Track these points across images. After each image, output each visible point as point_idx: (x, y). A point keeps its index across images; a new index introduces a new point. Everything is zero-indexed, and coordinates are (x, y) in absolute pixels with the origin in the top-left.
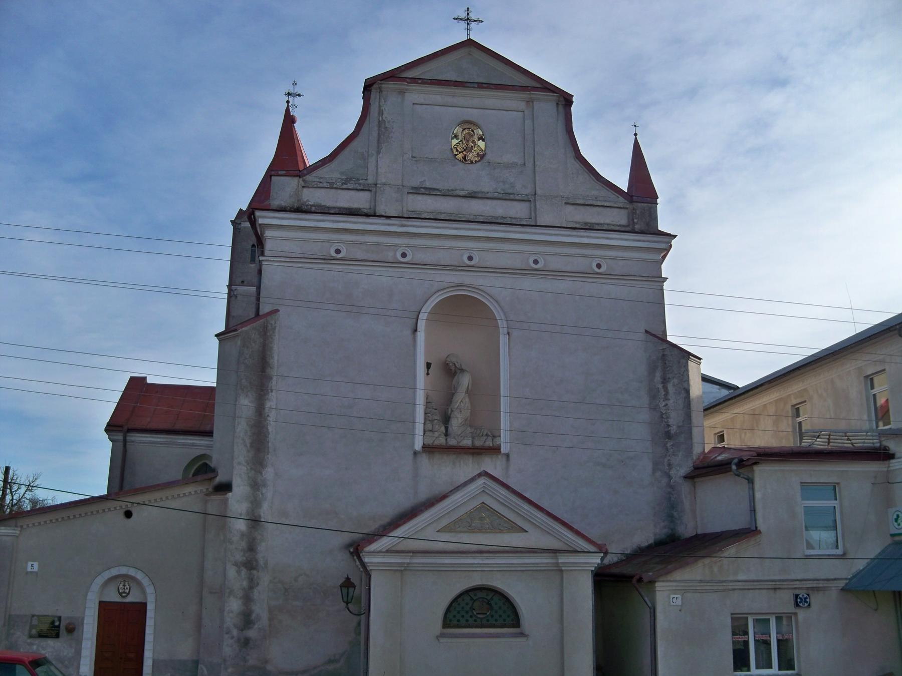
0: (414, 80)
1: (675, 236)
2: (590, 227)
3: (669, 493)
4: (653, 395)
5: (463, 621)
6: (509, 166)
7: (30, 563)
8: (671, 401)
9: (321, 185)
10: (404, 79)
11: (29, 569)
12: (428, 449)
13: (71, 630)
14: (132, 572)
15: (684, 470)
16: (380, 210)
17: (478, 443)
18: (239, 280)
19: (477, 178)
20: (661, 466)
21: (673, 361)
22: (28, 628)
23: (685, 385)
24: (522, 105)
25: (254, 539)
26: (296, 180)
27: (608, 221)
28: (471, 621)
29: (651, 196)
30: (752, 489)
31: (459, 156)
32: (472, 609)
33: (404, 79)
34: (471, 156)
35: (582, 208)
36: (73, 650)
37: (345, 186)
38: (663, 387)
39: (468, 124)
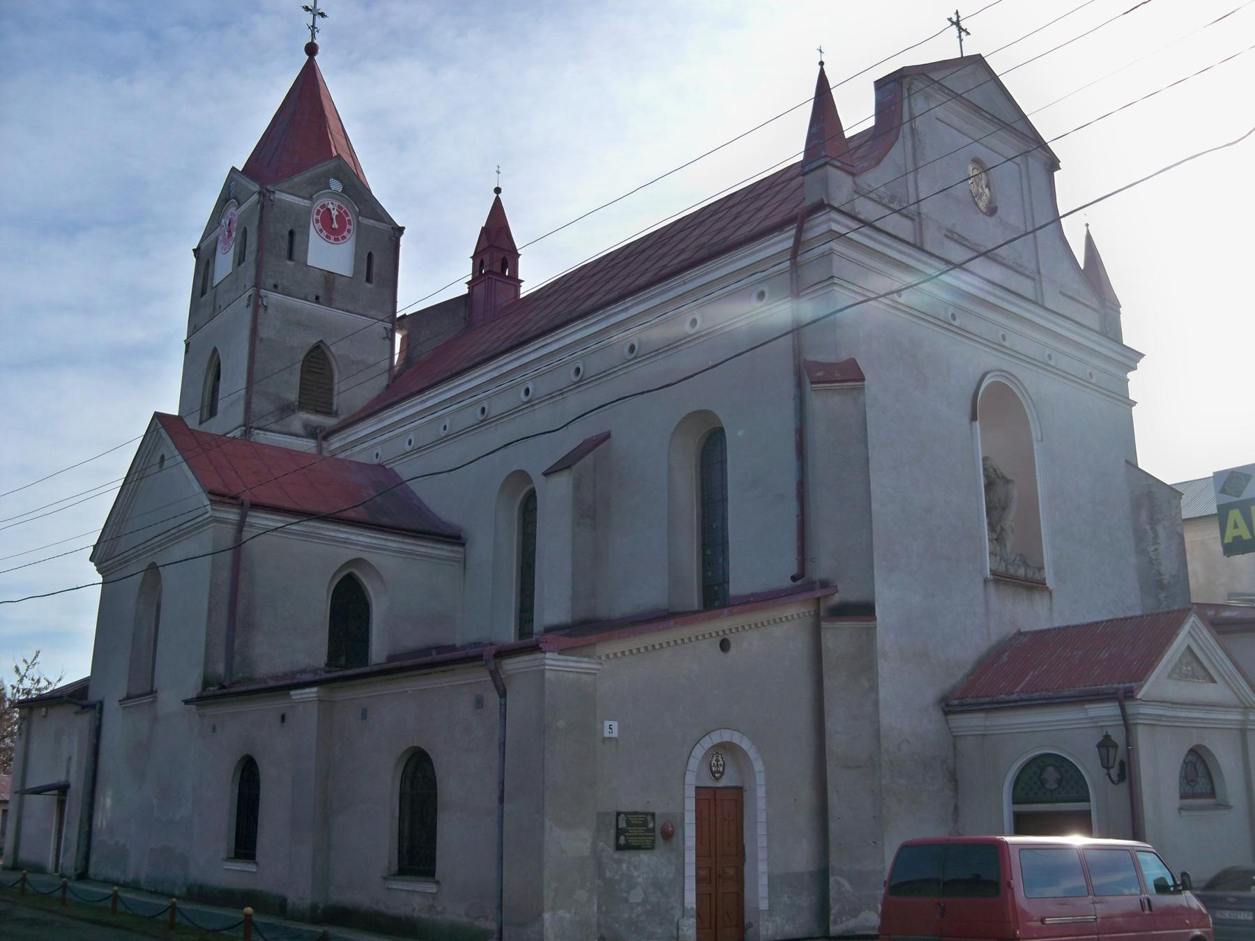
7: (607, 723)
8: (1162, 547)
11: (607, 735)
13: (668, 836)
22: (613, 832)
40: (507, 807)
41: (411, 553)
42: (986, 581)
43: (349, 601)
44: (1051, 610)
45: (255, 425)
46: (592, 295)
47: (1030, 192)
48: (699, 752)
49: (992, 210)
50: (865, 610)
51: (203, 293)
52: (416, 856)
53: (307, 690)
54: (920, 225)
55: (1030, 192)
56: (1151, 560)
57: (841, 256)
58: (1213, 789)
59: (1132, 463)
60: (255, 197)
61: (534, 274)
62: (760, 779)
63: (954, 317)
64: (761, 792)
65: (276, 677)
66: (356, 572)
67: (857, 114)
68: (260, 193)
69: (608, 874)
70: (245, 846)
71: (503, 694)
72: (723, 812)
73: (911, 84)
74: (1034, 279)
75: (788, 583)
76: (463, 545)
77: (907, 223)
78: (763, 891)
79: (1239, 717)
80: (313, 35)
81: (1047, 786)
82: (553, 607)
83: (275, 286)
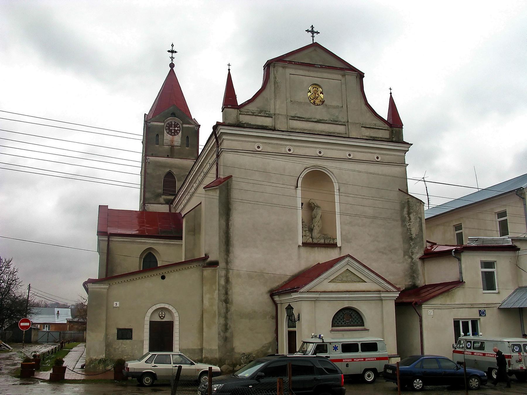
0: (290, 62)
1: (412, 144)
2: (374, 139)
3: (412, 266)
4: (403, 220)
5: (340, 324)
6: (337, 107)
7: (115, 303)
9: (248, 113)
10: (286, 61)
11: (115, 306)
12: (305, 244)
14: (167, 306)
15: (420, 254)
16: (278, 127)
17: (327, 242)
19: (319, 113)
20: (408, 253)
21: (410, 205)
23: (419, 216)
24: (340, 77)
25: (227, 288)
26: (236, 110)
27: (380, 136)
28: (343, 323)
29: (400, 125)
30: (460, 263)
31: (312, 101)
32: (343, 318)
33: (286, 61)
34: (317, 102)
35: (369, 130)
37: (260, 115)
38: (408, 216)
39: (316, 85)
41: (168, 244)
52: (292, 348)
66: (152, 252)
80: (172, 60)
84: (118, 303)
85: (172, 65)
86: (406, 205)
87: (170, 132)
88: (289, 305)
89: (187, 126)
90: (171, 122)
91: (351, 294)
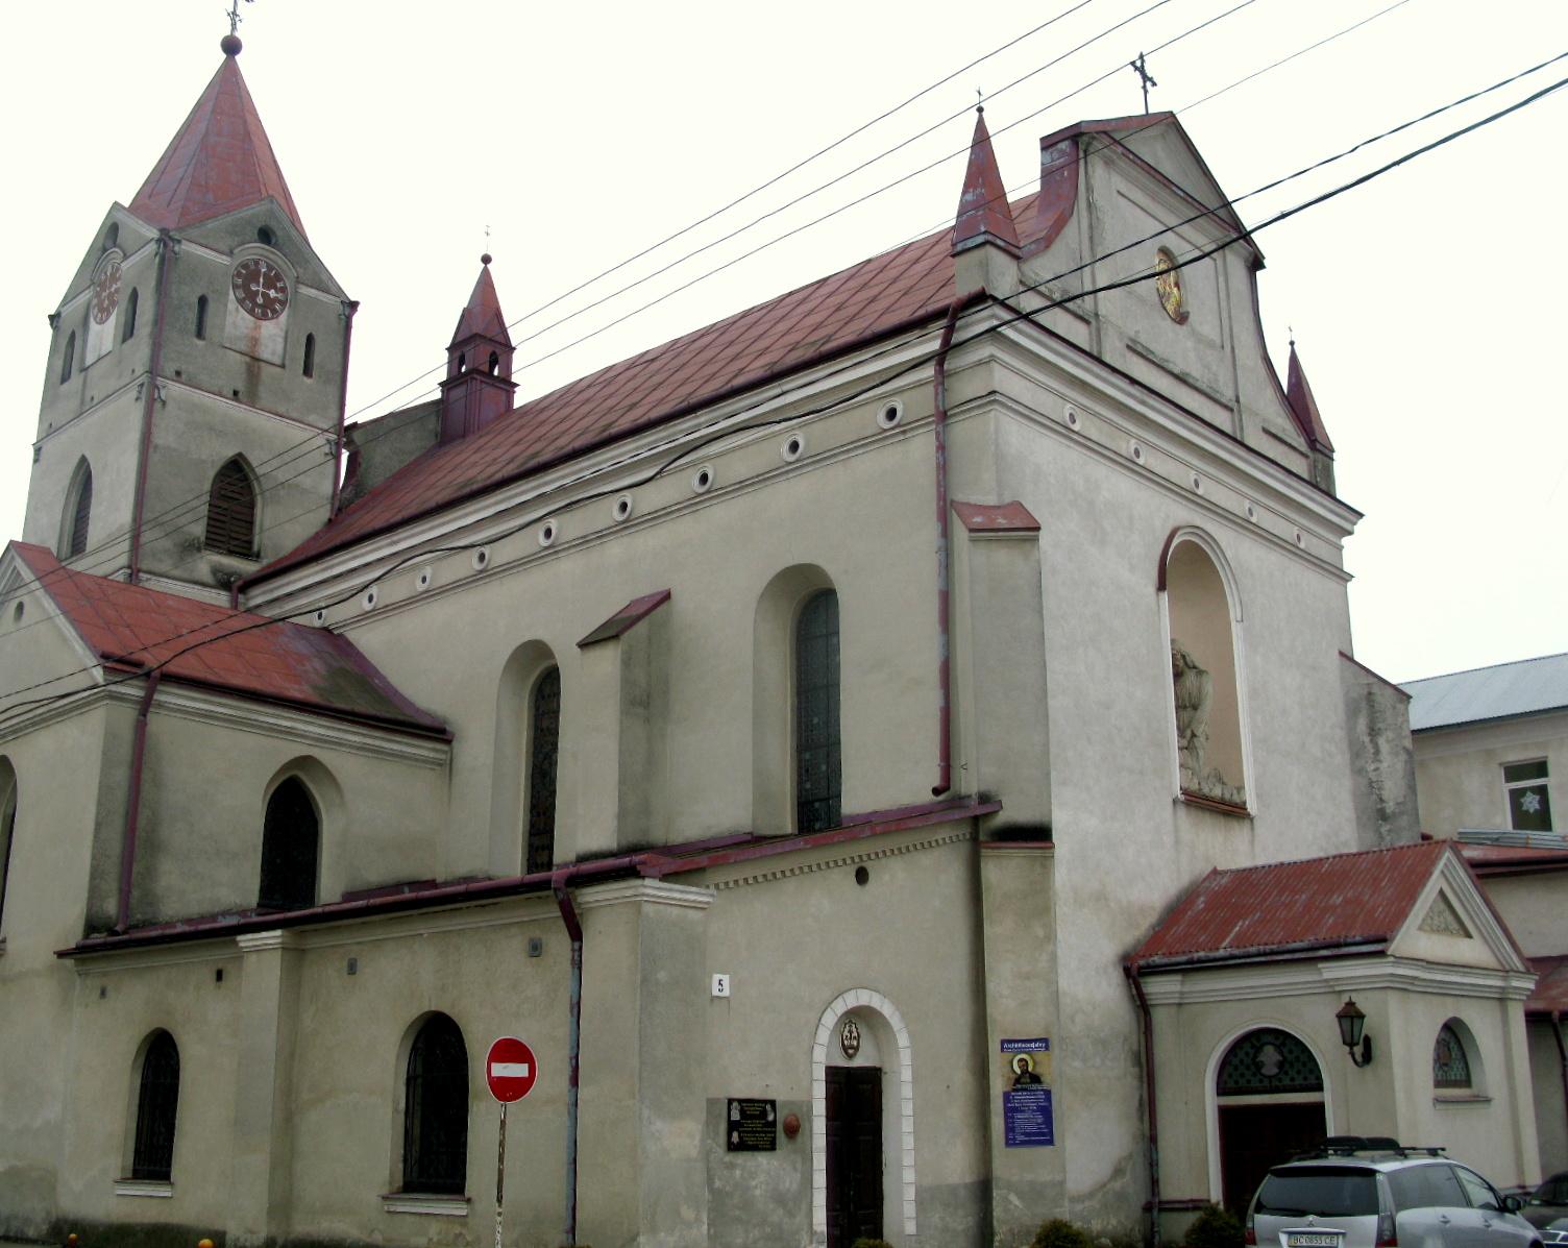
4: (1356, 753)
7: (717, 977)
8: (1385, 765)
11: (716, 993)
13: (792, 1131)
18: (170, 368)
36: (799, 1175)
38: (1371, 741)
40: (584, 1092)
42: (1175, 802)
43: (292, 816)
44: (1252, 842)
45: (144, 567)
46: (633, 406)
47: (1228, 296)
48: (830, 1019)
49: (1181, 318)
50: (1038, 835)
51: (65, 378)
53: (264, 934)
54: (1098, 330)
55: (1228, 296)
56: (1371, 783)
57: (1006, 366)
58: (1468, 1075)
59: (1347, 657)
60: (152, 247)
61: (536, 376)
62: (905, 1057)
63: (1137, 453)
64: (907, 1075)
65: (188, 921)
67: (1021, 176)
68: (159, 241)
69: (718, 1184)
70: (152, 1156)
71: (576, 934)
72: (856, 1099)
73: (1089, 144)
74: (1232, 410)
75: (927, 797)
76: (449, 742)
77: (1081, 327)
78: (910, 1209)
79: (1499, 983)
81: (1264, 1071)
82: (587, 825)
83: (178, 373)
84: (726, 979)
85: (231, 47)
86: (1364, 704)
87: (248, 300)
88: (1351, 1004)
89: (313, 292)
90: (256, 263)
91: (1465, 974)
